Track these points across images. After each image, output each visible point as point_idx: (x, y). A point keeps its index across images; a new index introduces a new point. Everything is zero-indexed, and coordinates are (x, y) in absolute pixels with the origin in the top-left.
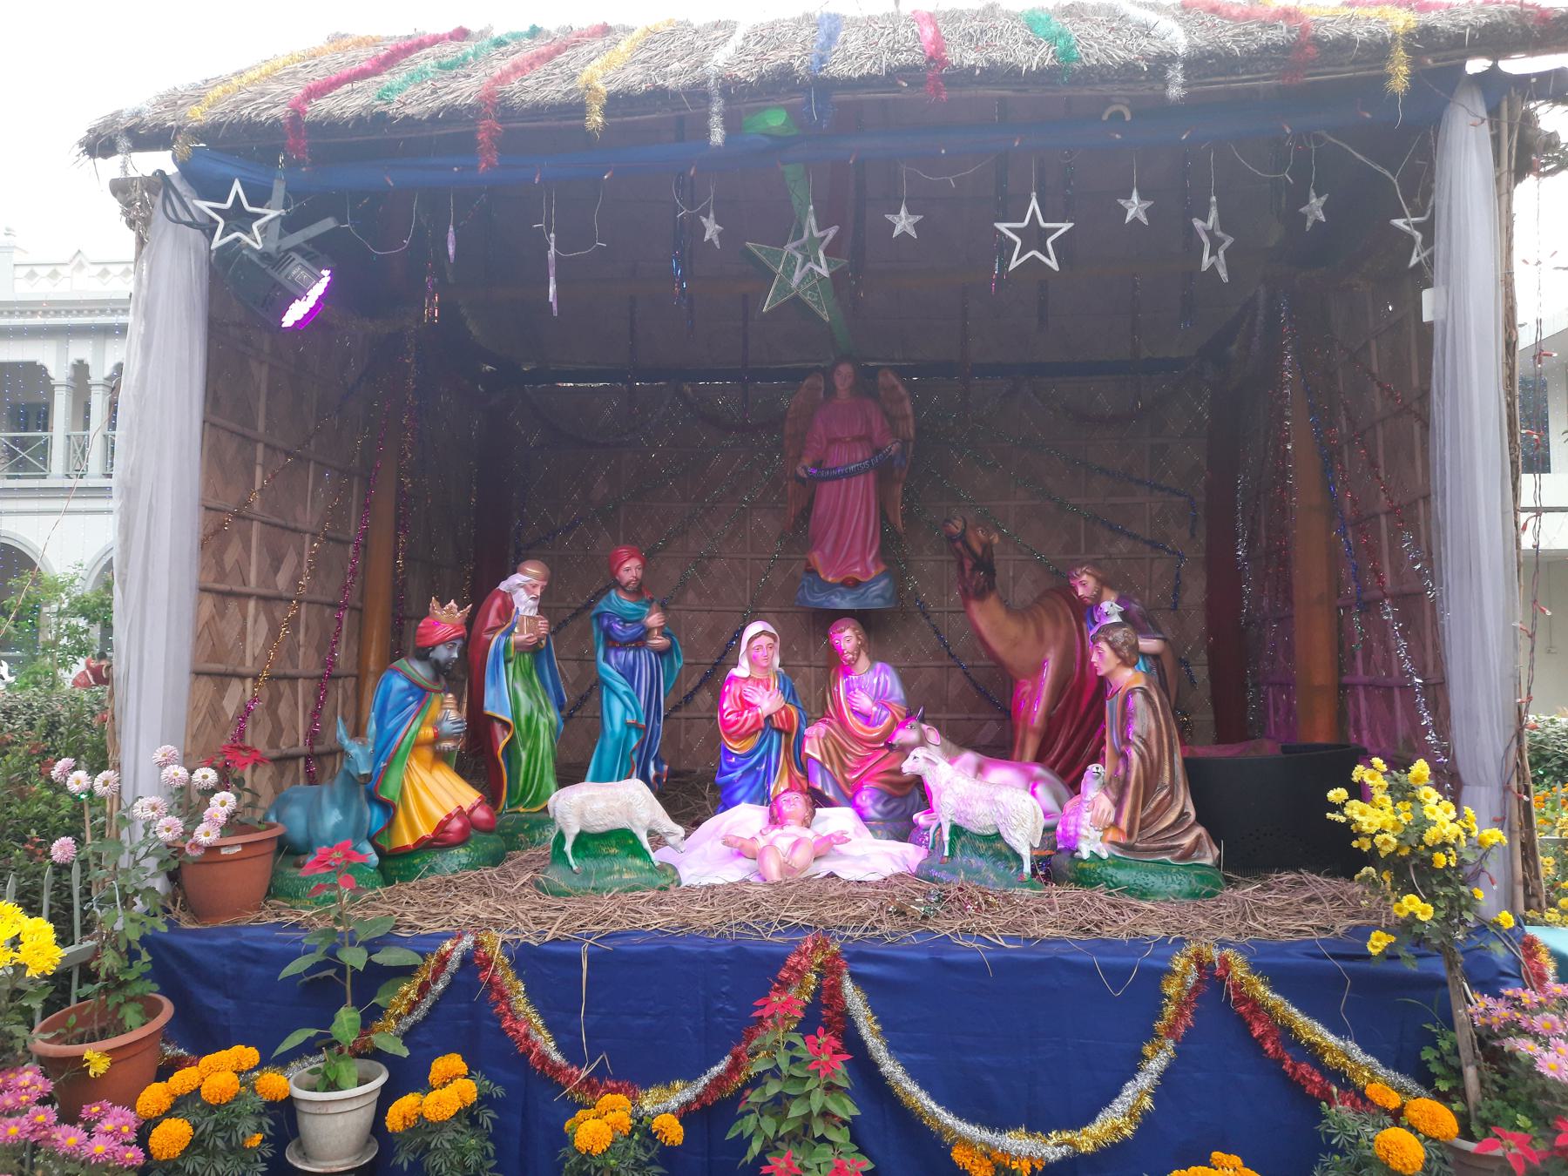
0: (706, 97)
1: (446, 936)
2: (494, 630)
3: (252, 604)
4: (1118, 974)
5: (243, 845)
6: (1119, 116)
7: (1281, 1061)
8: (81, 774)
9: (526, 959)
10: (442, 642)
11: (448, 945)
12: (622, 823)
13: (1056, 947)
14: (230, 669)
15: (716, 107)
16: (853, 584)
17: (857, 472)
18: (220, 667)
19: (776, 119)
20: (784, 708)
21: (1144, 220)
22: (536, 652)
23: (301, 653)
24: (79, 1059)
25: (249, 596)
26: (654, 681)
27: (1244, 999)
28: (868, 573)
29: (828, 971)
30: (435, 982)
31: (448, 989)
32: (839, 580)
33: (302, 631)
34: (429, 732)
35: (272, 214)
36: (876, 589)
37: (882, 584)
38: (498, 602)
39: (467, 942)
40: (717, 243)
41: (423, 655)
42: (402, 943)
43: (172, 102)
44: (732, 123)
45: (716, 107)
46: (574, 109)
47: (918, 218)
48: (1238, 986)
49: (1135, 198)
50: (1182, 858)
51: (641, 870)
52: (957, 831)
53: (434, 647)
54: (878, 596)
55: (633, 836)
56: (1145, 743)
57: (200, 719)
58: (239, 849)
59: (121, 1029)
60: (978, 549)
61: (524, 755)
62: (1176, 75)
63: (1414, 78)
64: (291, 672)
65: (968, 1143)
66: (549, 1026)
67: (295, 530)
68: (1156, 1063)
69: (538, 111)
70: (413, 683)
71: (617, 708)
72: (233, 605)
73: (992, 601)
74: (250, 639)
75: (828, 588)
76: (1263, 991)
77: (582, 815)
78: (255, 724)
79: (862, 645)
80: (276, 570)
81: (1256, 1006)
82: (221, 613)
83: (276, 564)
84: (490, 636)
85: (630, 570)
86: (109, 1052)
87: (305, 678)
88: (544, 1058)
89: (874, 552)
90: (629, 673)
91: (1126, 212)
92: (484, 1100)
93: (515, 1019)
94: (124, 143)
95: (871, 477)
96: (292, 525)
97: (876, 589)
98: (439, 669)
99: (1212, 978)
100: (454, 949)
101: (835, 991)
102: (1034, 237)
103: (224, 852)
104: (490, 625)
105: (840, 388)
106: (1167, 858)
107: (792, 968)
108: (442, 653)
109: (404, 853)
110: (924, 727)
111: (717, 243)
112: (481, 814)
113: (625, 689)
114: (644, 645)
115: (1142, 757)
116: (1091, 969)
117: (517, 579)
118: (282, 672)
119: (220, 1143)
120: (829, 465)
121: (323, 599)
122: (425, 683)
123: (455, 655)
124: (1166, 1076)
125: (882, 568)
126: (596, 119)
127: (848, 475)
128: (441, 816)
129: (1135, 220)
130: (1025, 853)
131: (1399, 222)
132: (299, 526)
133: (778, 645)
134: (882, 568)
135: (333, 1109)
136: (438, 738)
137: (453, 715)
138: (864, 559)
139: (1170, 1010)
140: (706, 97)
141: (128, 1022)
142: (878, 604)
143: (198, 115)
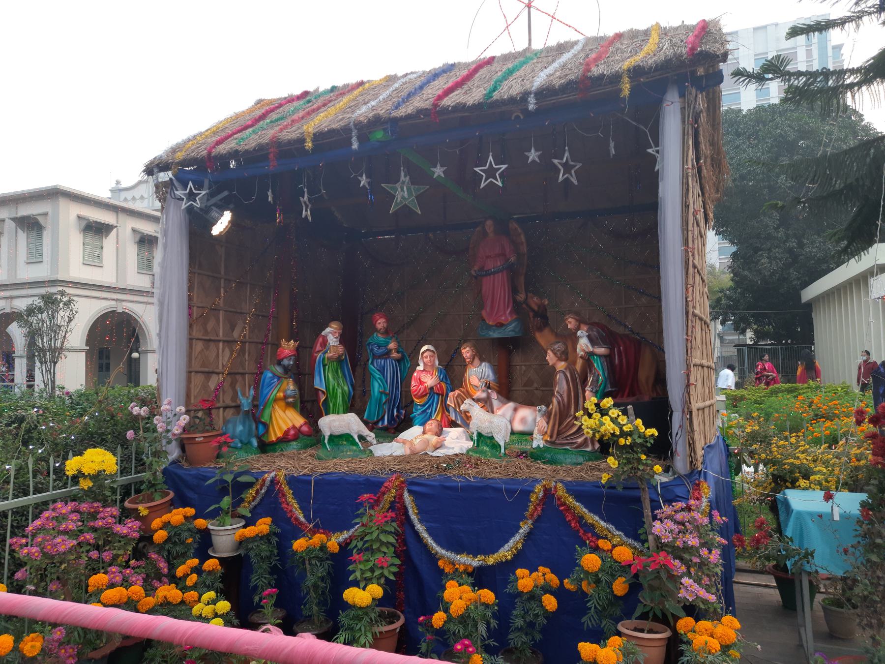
0: (350, 130)
1: (266, 473)
2: (319, 352)
3: (221, 345)
4: (510, 492)
5: (204, 437)
6: (518, 117)
7: (578, 531)
8: (137, 408)
9: (292, 481)
10: (285, 357)
11: (266, 475)
12: (347, 432)
13: (491, 481)
14: (211, 370)
15: (354, 133)
16: (500, 325)
17: (497, 272)
18: (206, 370)
19: (379, 135)
20: (439, 383)
21: (537, 160)
22: (339, 361)
23: (247, 363)
24: (137, 510)
25: (219, 341)
26: (394, 373)
27: (564, 504)
28: (507, 320)
29: (400, 488)
30: (261, 489)
31: (266, 492)
32: (494, 324)
33: (247, 354)
34: (281, 395)
35: (204, 193)
36: (511, 327)
37: (513, 325)
38: (321, 340)
39: (273, 474)
40: (367, 186)
41: (279, 363)
42: (251, 474)
43: (174, 150)
44: (362, 139)
45: (354, 133)
46: (301, 140)
47: (445, 168)
48: (559, 499)
49: (533, 151)
50: (576, 448)
51: (355, 451)
52: (480, 435)
53: (282, 360)
54: (513, 331)
55: (352, 437)
56: (561, 396)
57: (198, 390)
58: (202, 439)
59: (152, 500)
60: (536, 308)
61: (331, 405)
62: (532, 100)
63: (632, 90)
64: (241, 371)
65: (442, 557)
66: (301, 508)
67: (241, 313)
68: (525, 528)
69: (290, 142)
70: (274, 374)
71: (376, 385)
72: (212, 344)
73: (546, 332)
74: (221, 358)
75: (489, 327)
76: (571, 501)
77: (330, 428)
78: (224, 392)
79: (476, 354)
80: (233, 330)
81: (568, 508)
82: (207, 348)
83: (233, 328)
84: (316, 355)
85: (381, 323)
86: (148, 508)
87: (249, 374)
88: (297, 519)
89: (509, 310)
90: (382, 370)
91: (528, 158)
92: (272, 533)
93: (288, 504)
94: (156, 170)
95: (505, 272)
96: (239, 311)
97: (511, 327)
98: (286, 370)
99: (548, 494)
100: (268, 477)
101: (400, 497)
102: (491, 173)
103: (197, 439)
104: (317, 350)
105: (488, 231)
106: (568, 447)
107: (386, 487)
108: (286, 362)
109: (272, 444)
110: (490, 391)
111: (367, 186)
112: (305, 429)
113: (378, 376)
114: (389, 357)
115: (559, 403)
116: (500, 490)
117: (328, 330)
118: (237, 371)
119: (177, 540)
120: (485, 269)
121: (256, 340)
122: (279, 374)
123: (292, 363)
124: (529, 536)
125: (515, 317)
126: (309, 145)
127: (494, 273)
128: (285, 428)
129: (533, 161)
130: (502, 444)
131: (650, 151)
132: (243, 311)
133: (436, 355)
134: (515, 317)
135: (221, 533)
136: (285, 397)
137: (292, 388)
138: (505, 313)
139: (532, 507)
140: (350, 130)
141: (156, 499)
142: (512, 334)
143: (180, 156)
